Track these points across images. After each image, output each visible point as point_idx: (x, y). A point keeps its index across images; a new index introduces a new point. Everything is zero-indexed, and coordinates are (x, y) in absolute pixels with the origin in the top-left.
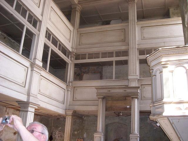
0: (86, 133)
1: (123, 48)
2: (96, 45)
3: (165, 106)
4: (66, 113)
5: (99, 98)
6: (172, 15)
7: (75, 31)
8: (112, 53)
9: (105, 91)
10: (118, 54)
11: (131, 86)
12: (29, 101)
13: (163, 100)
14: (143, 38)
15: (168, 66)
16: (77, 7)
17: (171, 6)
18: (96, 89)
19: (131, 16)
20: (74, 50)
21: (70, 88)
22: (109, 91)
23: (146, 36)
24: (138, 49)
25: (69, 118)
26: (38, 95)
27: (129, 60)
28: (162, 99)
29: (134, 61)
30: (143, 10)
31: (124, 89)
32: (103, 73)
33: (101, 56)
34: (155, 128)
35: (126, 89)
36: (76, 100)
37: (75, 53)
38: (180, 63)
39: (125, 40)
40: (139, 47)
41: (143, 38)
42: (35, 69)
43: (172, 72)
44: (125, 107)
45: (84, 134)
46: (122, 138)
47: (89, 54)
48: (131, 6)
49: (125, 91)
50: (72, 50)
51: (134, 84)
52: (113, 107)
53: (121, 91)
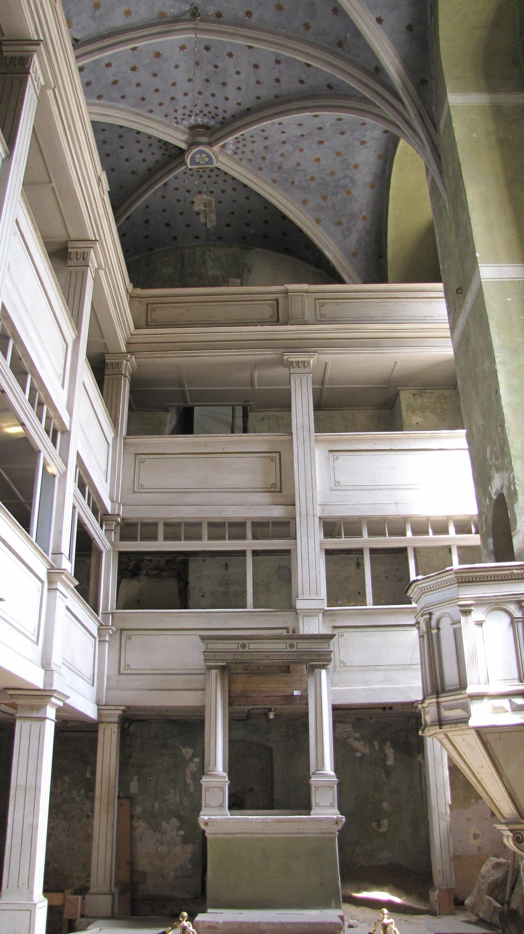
0: (135, 778)
1: (278, 512)
2: (190, 498)
3: (305, 633)
4: (99, 715)
5: (209, 668)
6: (407, 410)
7: (120, 443)
8: (241, 525)
9: (232, 646)
10: (262, 528)
11: (305, 633)
12: (52, 685)
13: (465, 688)
14: (336, 486)
15: (472, 610)
16: (125, 362)
17: (407, 386)
18: (203, 638)
19: (300, 414)
20: (119, 510)
21: (110, 632)
22: (244, 646)
23: (344, 479)
24: (320, 518)
25: (108, 732)
26: (63, 667)
27: (296, 549)
28: (462, 685)
29: (312, 556)
30: (322, 389)
31: (289, 642)
32: (192, 578)
33: (205, 531)
34: (358, 754)
35: (294, 642)
36: (128, 672)
37: (123, 519)
38: (496, 605)
39: (281, 486)
40: (326, 514)
41: (336, 486)
42: (59, 586)
43: (480, 624)
44: (290, 694)
45: (132, 780)
46: (251, 790)
47: (166, 525)
48: (298, 381)
49: (292, 646)
50: (113, 508)
51: (312, 626)
52: (251, 694)
53: (280, 646)
